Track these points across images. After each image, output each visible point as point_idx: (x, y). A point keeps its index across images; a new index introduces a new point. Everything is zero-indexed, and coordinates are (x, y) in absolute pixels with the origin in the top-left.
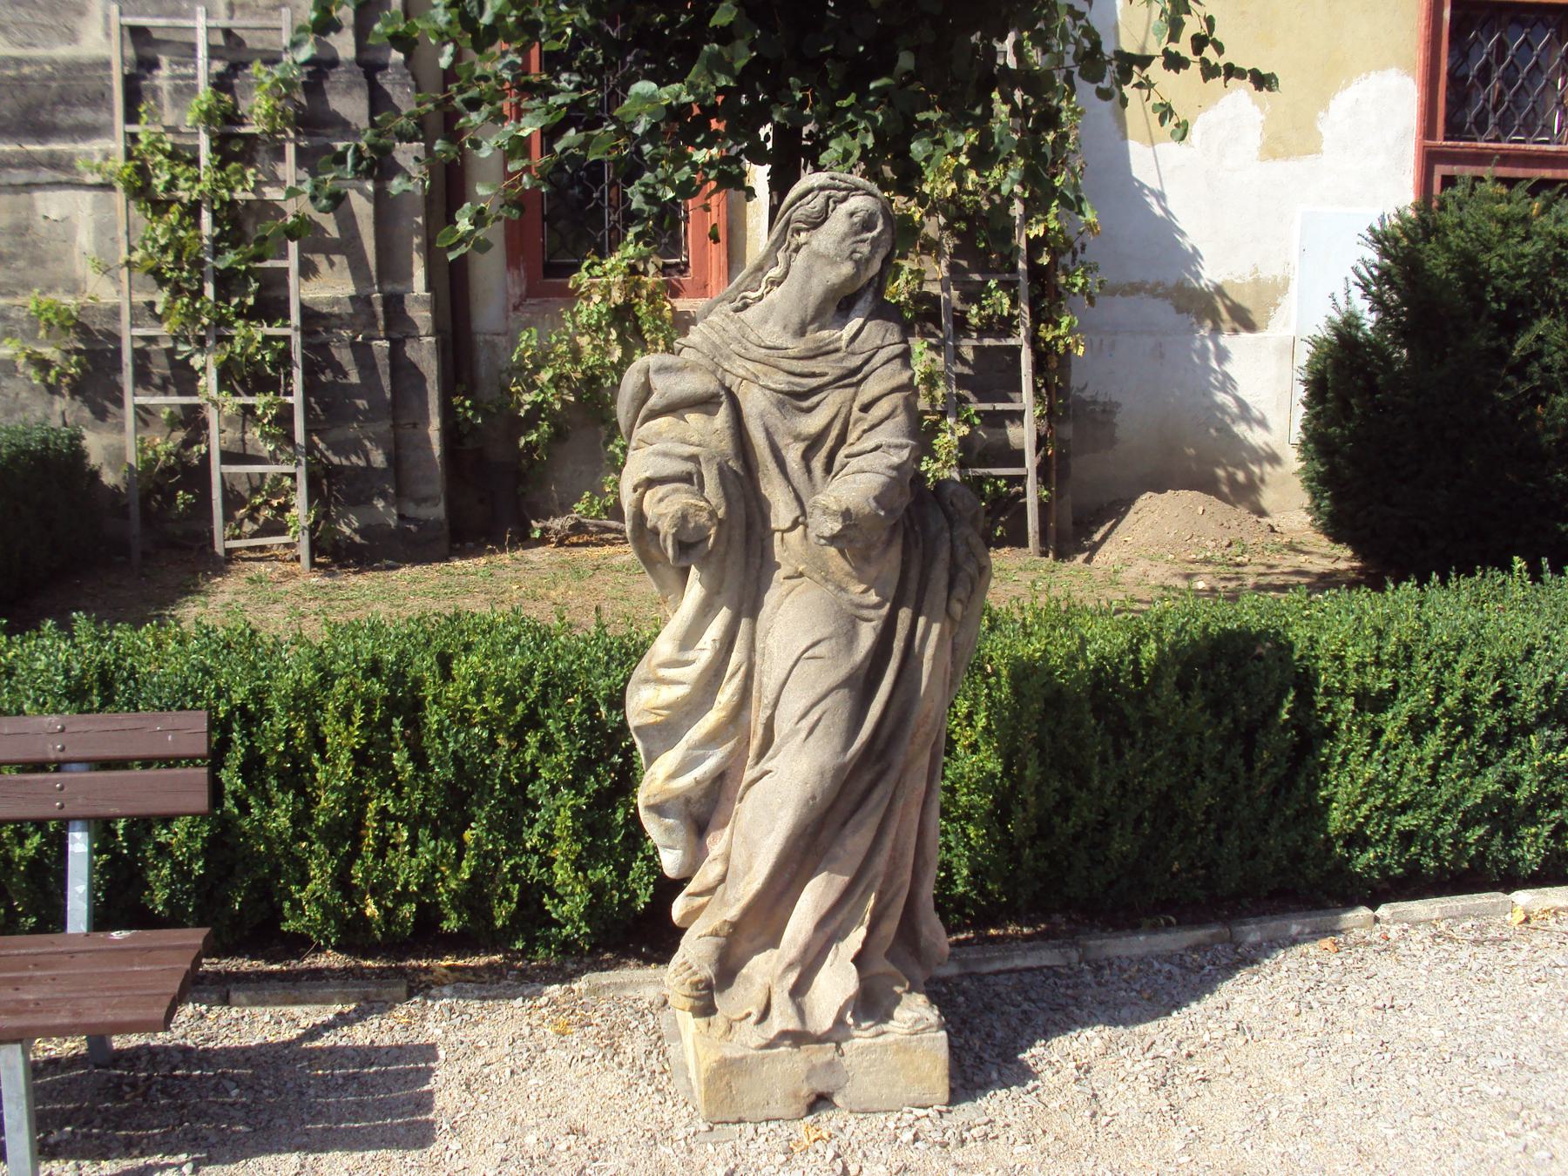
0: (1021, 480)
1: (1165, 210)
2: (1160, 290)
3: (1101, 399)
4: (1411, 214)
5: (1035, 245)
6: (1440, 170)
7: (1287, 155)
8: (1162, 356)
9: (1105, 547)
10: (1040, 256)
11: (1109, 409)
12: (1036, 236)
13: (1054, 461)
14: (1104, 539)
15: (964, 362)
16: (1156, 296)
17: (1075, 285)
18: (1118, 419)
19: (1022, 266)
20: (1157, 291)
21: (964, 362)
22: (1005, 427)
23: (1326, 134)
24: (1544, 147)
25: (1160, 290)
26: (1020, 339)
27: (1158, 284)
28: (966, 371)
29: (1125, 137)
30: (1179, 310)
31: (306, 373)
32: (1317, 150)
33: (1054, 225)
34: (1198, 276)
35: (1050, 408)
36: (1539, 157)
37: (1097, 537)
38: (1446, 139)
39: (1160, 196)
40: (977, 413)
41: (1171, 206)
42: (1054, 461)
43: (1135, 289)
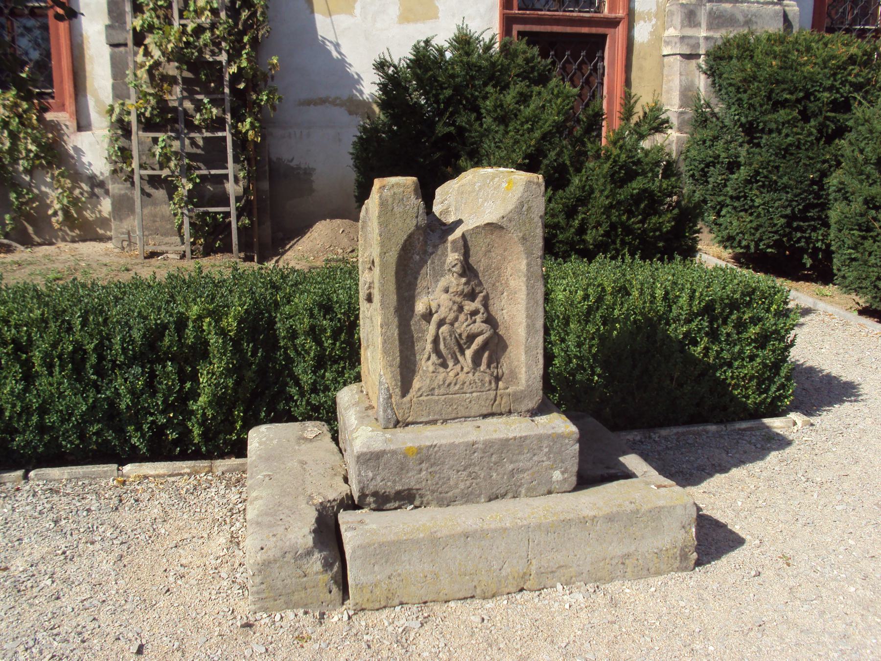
0: (227, 215)
1: (340, 53)
2: (338, 102)
3: (303, 166)
4: (412, 57)
5: (235, 78)
6: (516, 28)
7: (416, 21)
8: (340, 140)
9: (289, 253)
10: (240, 83)
11: (308, 172)
12: (234, 73)
13: (255, 203)
14: (291, 247)
15: (198, 146)
16: (336, 105)
17: (262, 100)
18: (314, 178)
19: (227, 90)
20: (335, 102)
21: (198, 146)
22: (223, 184)
23: (441, 8)
24: (571, 14)
25: (338, 102)
26: (228, 134)
27: (337, 98)
28: (199, 151)
29: (312, 12)
30: (351, 113)
31: (601, 134)
32: (436, 17)
33: (244, 64)
34: (361, 93)
35: (249, 173)
36: (555, 19)
37: (288, 247)
38: (519, 9)
39: (337, 46)
40: (197, 176)
41: (343, 51)
42: (255, 203)
43: (323, 101)
